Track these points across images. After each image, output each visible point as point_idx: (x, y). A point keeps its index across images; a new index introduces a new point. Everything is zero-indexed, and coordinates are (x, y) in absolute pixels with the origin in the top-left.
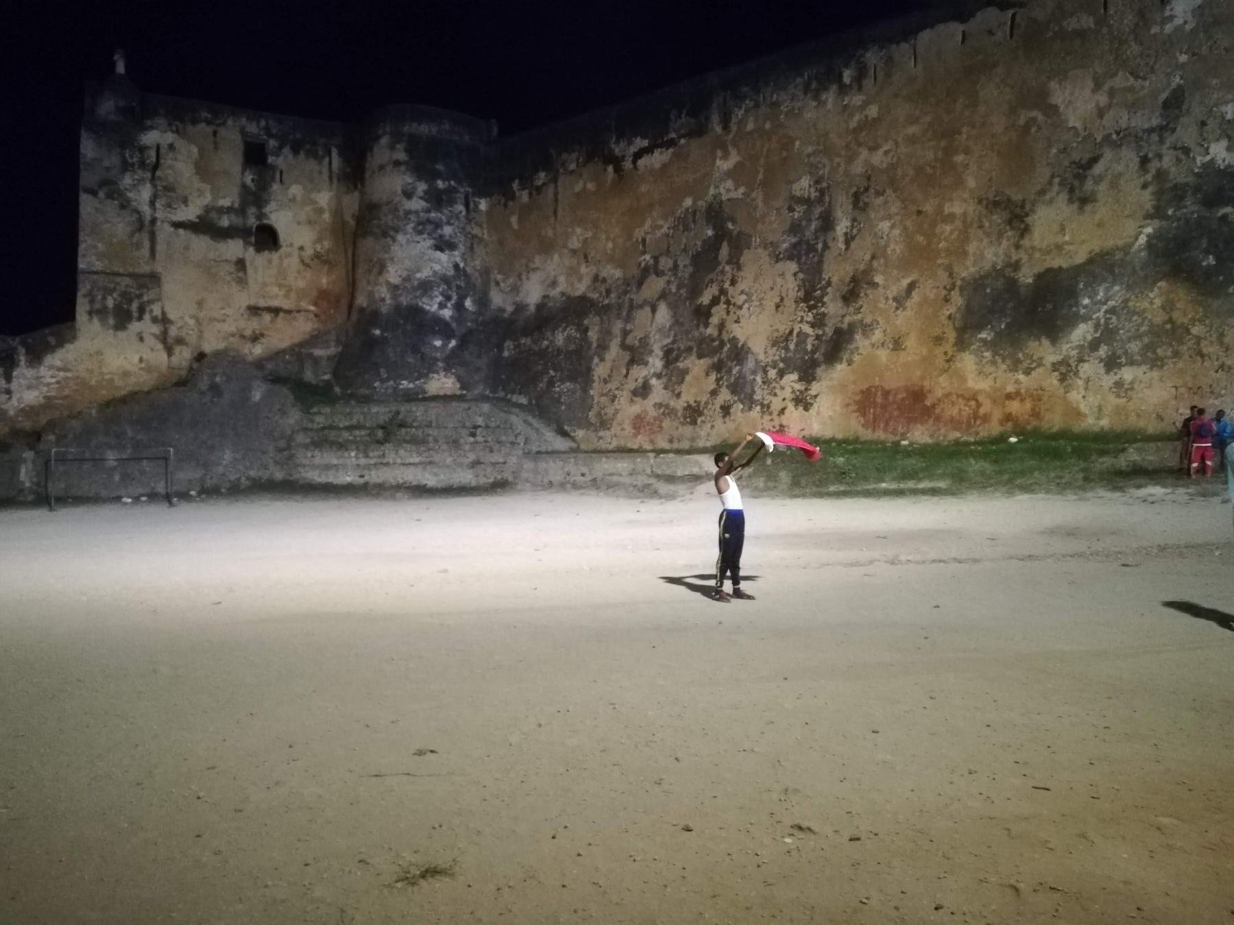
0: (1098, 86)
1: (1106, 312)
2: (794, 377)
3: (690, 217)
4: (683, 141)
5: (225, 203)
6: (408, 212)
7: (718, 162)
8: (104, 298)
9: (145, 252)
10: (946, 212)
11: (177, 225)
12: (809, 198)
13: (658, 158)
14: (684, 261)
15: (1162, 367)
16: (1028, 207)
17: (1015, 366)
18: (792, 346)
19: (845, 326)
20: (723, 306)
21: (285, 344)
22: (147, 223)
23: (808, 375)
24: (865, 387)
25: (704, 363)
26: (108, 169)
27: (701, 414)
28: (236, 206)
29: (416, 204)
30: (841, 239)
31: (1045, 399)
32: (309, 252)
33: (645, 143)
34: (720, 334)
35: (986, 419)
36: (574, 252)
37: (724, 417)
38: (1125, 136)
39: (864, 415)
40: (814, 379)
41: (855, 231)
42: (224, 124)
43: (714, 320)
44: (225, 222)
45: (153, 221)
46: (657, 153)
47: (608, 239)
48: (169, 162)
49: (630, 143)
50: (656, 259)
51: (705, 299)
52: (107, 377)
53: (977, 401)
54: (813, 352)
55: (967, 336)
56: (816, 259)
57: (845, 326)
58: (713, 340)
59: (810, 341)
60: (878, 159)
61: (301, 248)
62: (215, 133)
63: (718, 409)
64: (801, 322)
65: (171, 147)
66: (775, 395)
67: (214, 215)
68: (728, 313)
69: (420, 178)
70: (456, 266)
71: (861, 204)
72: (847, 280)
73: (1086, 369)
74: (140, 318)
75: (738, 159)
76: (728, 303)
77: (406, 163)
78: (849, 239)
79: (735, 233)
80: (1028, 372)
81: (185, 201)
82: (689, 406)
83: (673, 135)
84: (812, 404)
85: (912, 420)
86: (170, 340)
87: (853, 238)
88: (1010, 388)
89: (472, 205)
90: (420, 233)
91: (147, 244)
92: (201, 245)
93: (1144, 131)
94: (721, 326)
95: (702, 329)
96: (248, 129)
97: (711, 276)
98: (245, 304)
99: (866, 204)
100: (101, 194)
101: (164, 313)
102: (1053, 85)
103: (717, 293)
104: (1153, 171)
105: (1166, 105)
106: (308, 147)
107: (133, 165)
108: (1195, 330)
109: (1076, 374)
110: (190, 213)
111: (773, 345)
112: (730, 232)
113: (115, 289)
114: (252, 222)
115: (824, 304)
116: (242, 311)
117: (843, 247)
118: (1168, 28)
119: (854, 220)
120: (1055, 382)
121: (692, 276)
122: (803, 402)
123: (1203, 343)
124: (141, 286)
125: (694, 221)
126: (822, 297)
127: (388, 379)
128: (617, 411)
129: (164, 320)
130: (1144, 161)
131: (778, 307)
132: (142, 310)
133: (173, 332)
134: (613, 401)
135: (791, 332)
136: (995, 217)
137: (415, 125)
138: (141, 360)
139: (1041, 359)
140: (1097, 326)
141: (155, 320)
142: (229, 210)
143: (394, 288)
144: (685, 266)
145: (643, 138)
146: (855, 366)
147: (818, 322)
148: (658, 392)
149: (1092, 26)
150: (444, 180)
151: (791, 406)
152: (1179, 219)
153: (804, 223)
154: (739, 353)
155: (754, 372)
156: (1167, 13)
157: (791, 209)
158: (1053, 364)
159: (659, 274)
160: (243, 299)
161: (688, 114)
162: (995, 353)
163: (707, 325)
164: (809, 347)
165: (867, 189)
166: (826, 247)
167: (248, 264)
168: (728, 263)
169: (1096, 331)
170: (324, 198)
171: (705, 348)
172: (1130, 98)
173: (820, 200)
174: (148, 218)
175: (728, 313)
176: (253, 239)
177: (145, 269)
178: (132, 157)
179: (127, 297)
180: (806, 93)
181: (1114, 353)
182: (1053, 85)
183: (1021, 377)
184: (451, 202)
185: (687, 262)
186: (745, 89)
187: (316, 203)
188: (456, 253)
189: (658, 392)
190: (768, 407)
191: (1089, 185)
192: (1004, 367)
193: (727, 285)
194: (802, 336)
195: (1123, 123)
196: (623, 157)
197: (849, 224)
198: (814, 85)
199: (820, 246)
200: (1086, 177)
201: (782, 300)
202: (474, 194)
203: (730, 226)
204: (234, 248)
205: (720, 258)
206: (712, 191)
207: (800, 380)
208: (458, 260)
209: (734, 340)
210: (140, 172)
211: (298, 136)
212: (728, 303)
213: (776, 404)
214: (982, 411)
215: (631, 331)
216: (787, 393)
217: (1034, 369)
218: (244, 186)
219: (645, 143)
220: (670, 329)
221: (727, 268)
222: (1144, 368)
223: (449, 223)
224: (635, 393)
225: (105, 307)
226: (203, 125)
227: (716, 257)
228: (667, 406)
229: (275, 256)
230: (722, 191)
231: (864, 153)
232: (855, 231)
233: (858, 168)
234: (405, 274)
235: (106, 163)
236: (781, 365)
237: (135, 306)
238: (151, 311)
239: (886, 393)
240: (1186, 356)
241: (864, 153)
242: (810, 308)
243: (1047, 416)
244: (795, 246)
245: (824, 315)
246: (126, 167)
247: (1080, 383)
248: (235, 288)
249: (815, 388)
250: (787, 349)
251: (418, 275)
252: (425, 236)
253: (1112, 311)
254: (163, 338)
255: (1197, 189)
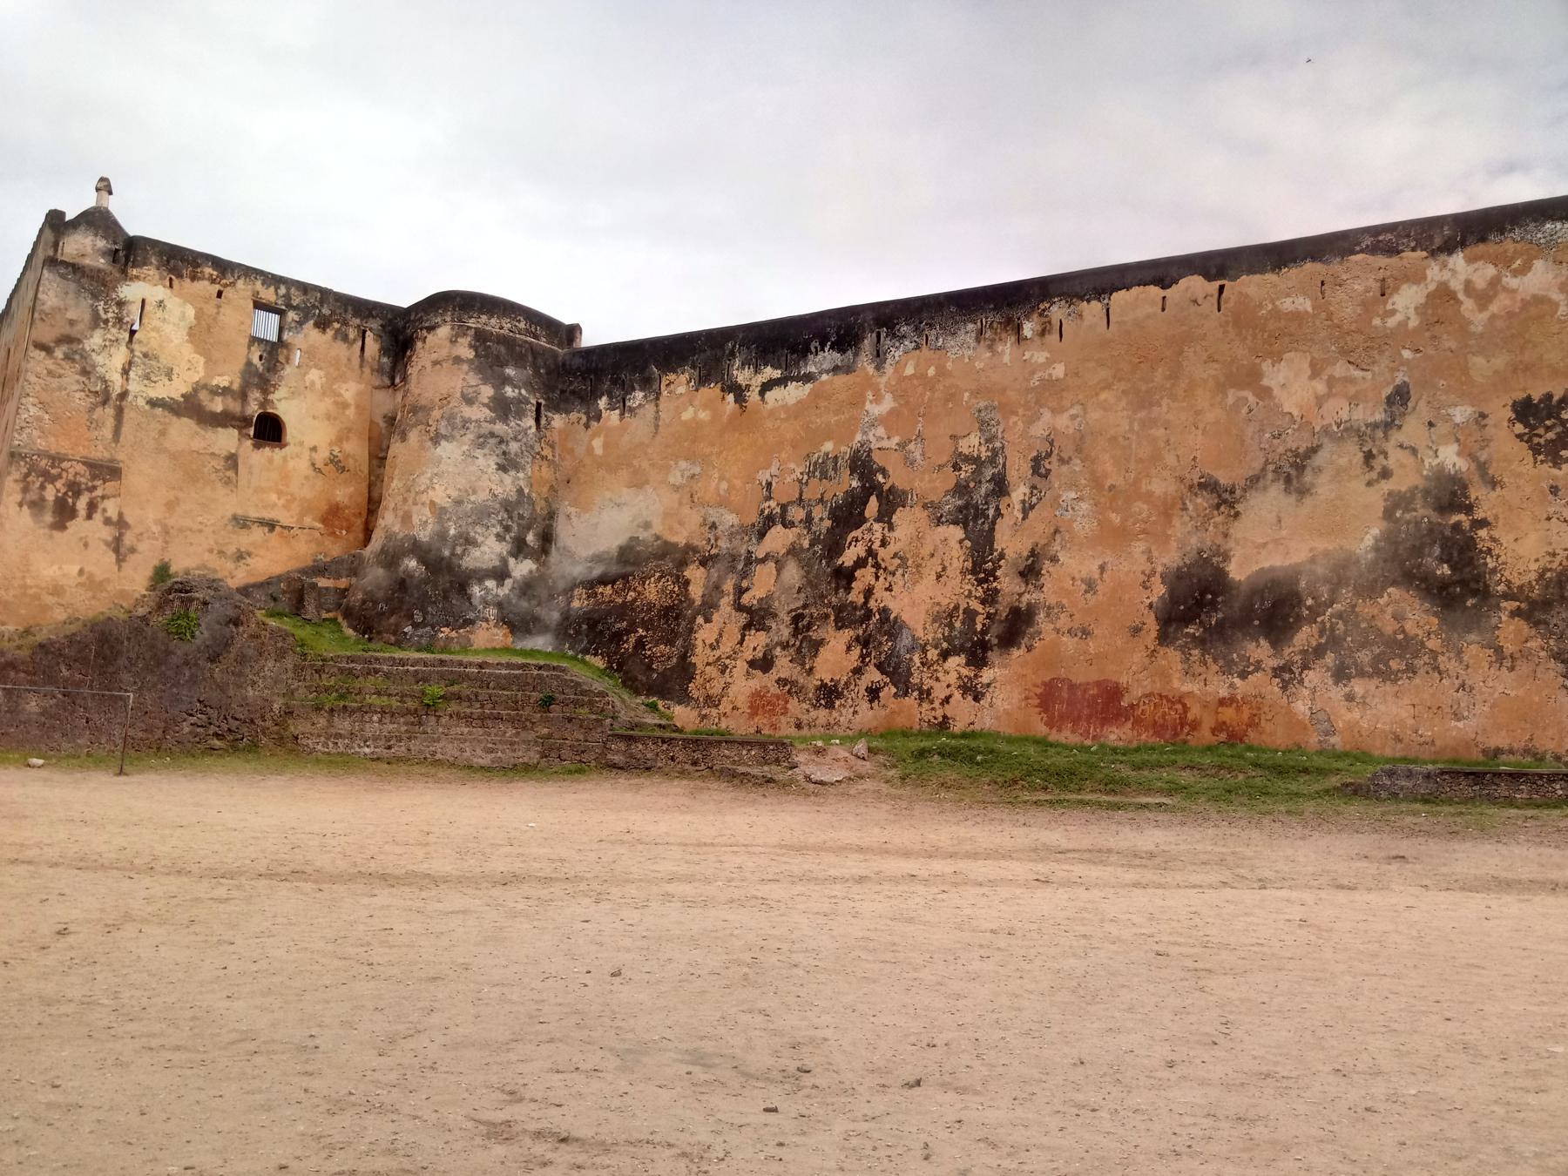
0: (1315, 373)
1: (1332, 616)
2: (961, 659)
3: (830, 465)
4: (825, 377)
5: (223, 381)
6: (466, 422)
7: (868, 406)
8: (42, 487)
9: (108, 433)
10: (1144, 489)
11: (153, 403)
12: (979, 457)
13: (794, 393)
14: (819, 512)
15: (1395, 681)
16: (1238, 492)
17: (1227, 669)
18: (958, 625)
19: (1023, 606)
20: (870, 570)
21: (277, 569)
22: (114, 396)
23: (977, 655)
24: (1047, 679)
25: (847, 634)
26: (72, 323)
27: (839, 695)
28: (236, 387)
29: (478, 413)
30: (1018, 506)
31: (1266, 709)
32: (323, 455)
33: (777, 374)
34: (866, 603)
35: (1195, 726)
36: (676, 488)
37: (871, 701)
38: (1346, 430)
39: (1046, 711)
40: (985, 664)
41: (1034, 500)
42: (233, 284)
43: (858, 586)
44: (218, 405)
45: (124, 395)
46: (792, 386)
47: (721, 478)
48: (155, 323)
49: (757, 371)
50: (784, 508)
51: (848, 558)
52: (31, 592)
53: (1184, 705)
54: (984, 632)
55: (1171, 630)
56: (986, 527)
57: (1023, 606)
58: (855, 608)
59: (979, 619)
60: (1062, 422)
61: (314, 449)
62: (220, 294)
63: (862, 692)
64: (969, 596)
65: (161, 304)
66: (937, 679)
67: (203, 396)
68: (877, 578)
69: (485, 381)
70: (520, 491)
71: (1043, 471)
72: (1025, 554)
73: (1311, 677)
74: (89, 517)
75: (893, 404)
76: (877, 566)
77: (470, 362)
78: (1027, 508)
79: (886, 488)
80: (1244, 675)
81: (169, 374)
82: (823, 686)
83: (812, 369)
84: (983, 694)
85: (1105, 721)
86: (122, 550)
87: (1032, 507)
88: (1224, 692)
89: (543, 421)
90: (481, 446)
91: (110, 422)
92: (183, 431)
93: (1367, 426)
94: (868, 593)
95: (841, 592)
96: (262, 295)
97: (853, 534)
98: (229, 514)
99: (1048, 471)
100: (59, 353)
101: (121, 515)
102: (1266, 366)
103: (863, 554)
104: (1378, 469)
105: (1390, 401)
106: (336, 325)
107: (106, 322)
108: (1431, 644)
109: (1301, 682)
110: (174, 390)
111: (934, 621)
112: (881, 485)
113: (60, 476)
114: (253, 409)
115: (996, 578)
116: (225, 521)
117: (1020, 516)
118: (1392, 322)
119: (1034, 487)
120: (1276, 689)
121: (830, 531)
122: (973, 691)
123: (1440, 658)
124: (94, 477)
125: (835, 469)
126: (994, 570)
127: (423, 625)
128: (727, 686)
129: (121, 524)
130: (1369, 457)
131: (939, 577)
132: (92, 507)
133: (128, 539)
134: (723, 672)
135: (956, 608)
136: (1199, 500)
137: (484, 318)
138: (81, 572)
139: (1259, 662)
140: (1322, 632)
141: (107, 521)
142: (225, 391)
143: (439, 512)
144: (821, 519)
145: (775, 367)
146: (1035, 652)
147: (990, 598)
148: (784, 666)
149: (1310, 309)
150: (514, 386)
151: (957, 695)
152: (1408, 523)
153: (972, 485)
154: (890, 625)
155: (911, 650)
156: (1389, 307)
157: (956, 467)
158: (1274, 669)
159: (787, 525)
160: (229, 503)
161: (832, 347)
162: (1205, 652)
163: (848, 589)
164: (979, 627)
165: (1049, 455)
166: (998, 513)
167: (240, 462)
168: (878, 520)
169: (1321, 636)
170: (350, 390)
171: (844, 617)
172: (1352, 390)
173: (992, 461)
174: (117, 389)
175: (877, 578)
176: (252, 432)
177: (99, 453)
178: (106, 312)
179: (75, 489)
180: (978, 340)
181: (1342, 663)
182: (1266, 366)
183: (1237, 681)
184: (520, 415)
185: (825, 515)
186: (904, 328)
187: (340, 395)
188: (521, 475)
189: (784, 666)
190: (929, 693)
191: (1308, 477)
192: (1215, 668)
193: (876, 546)
194: (970, 615)
195: (1344, 415)
196: (748, 386)
197: (1028, 491)
198: (989, 334)
199: (991, 512)
200: (1304, 467)
201: (944, 569)
202: (548, 408)
203: (880, 478)
204: (227, 440)
205: (867, 514)
206: (859, 437)
207: (968, 664)
208: (522, 483)
209: (885, 611)
210: (114, 331)
211: (325, 311)
212: (877, 566)
213: (939, 692)
214: (1190, 716)
215: (747, 589)
216: (952, 678)
217: (1251, 673)
218: (249, 363)
219: (777, 374)
220: (799, 591)
221: (877, 527)
222: (1376, 681)
223: (515, 439)
224: (752, 664)
225: (43, 499)
226: (206, 283)
227: (862, 513)
228: (794, 683)
229: (277, 454)
230: (871, 438)
231: (1047, 415)
232: (1034, 500)
233: (1039, 430)
234: (455, 494)
235: (71, 315)
236: (945, 645)
237: (82, 504)
238: (104, 510)
239: (1072, 687)
240: (1422, 672)
241: (1047, 415)
242: (980, 582)
243: (1267, 727)
244: (960, 509)
245: (996, 591)
246: (97, 321)
247: (1306, 692)
248: (221, 490)
249: (987, 675)
250: (951, 626)
251: (473, 498)
252: (486, 451)
253: (1340, 616)
254: (116, 545)
255: (1426, 492)
